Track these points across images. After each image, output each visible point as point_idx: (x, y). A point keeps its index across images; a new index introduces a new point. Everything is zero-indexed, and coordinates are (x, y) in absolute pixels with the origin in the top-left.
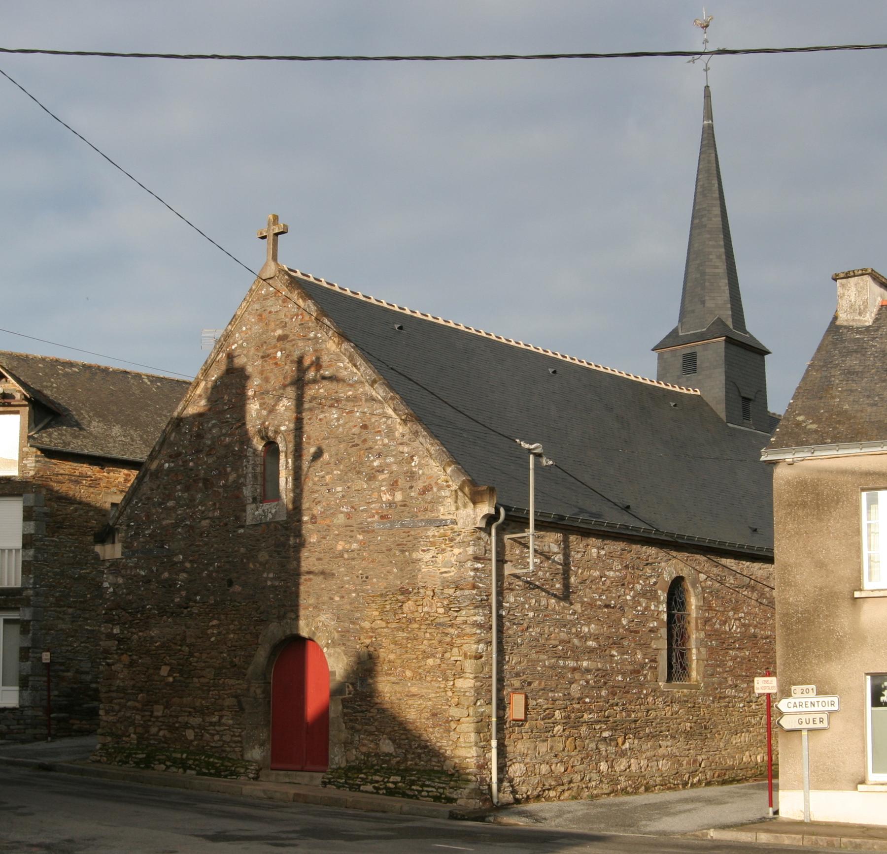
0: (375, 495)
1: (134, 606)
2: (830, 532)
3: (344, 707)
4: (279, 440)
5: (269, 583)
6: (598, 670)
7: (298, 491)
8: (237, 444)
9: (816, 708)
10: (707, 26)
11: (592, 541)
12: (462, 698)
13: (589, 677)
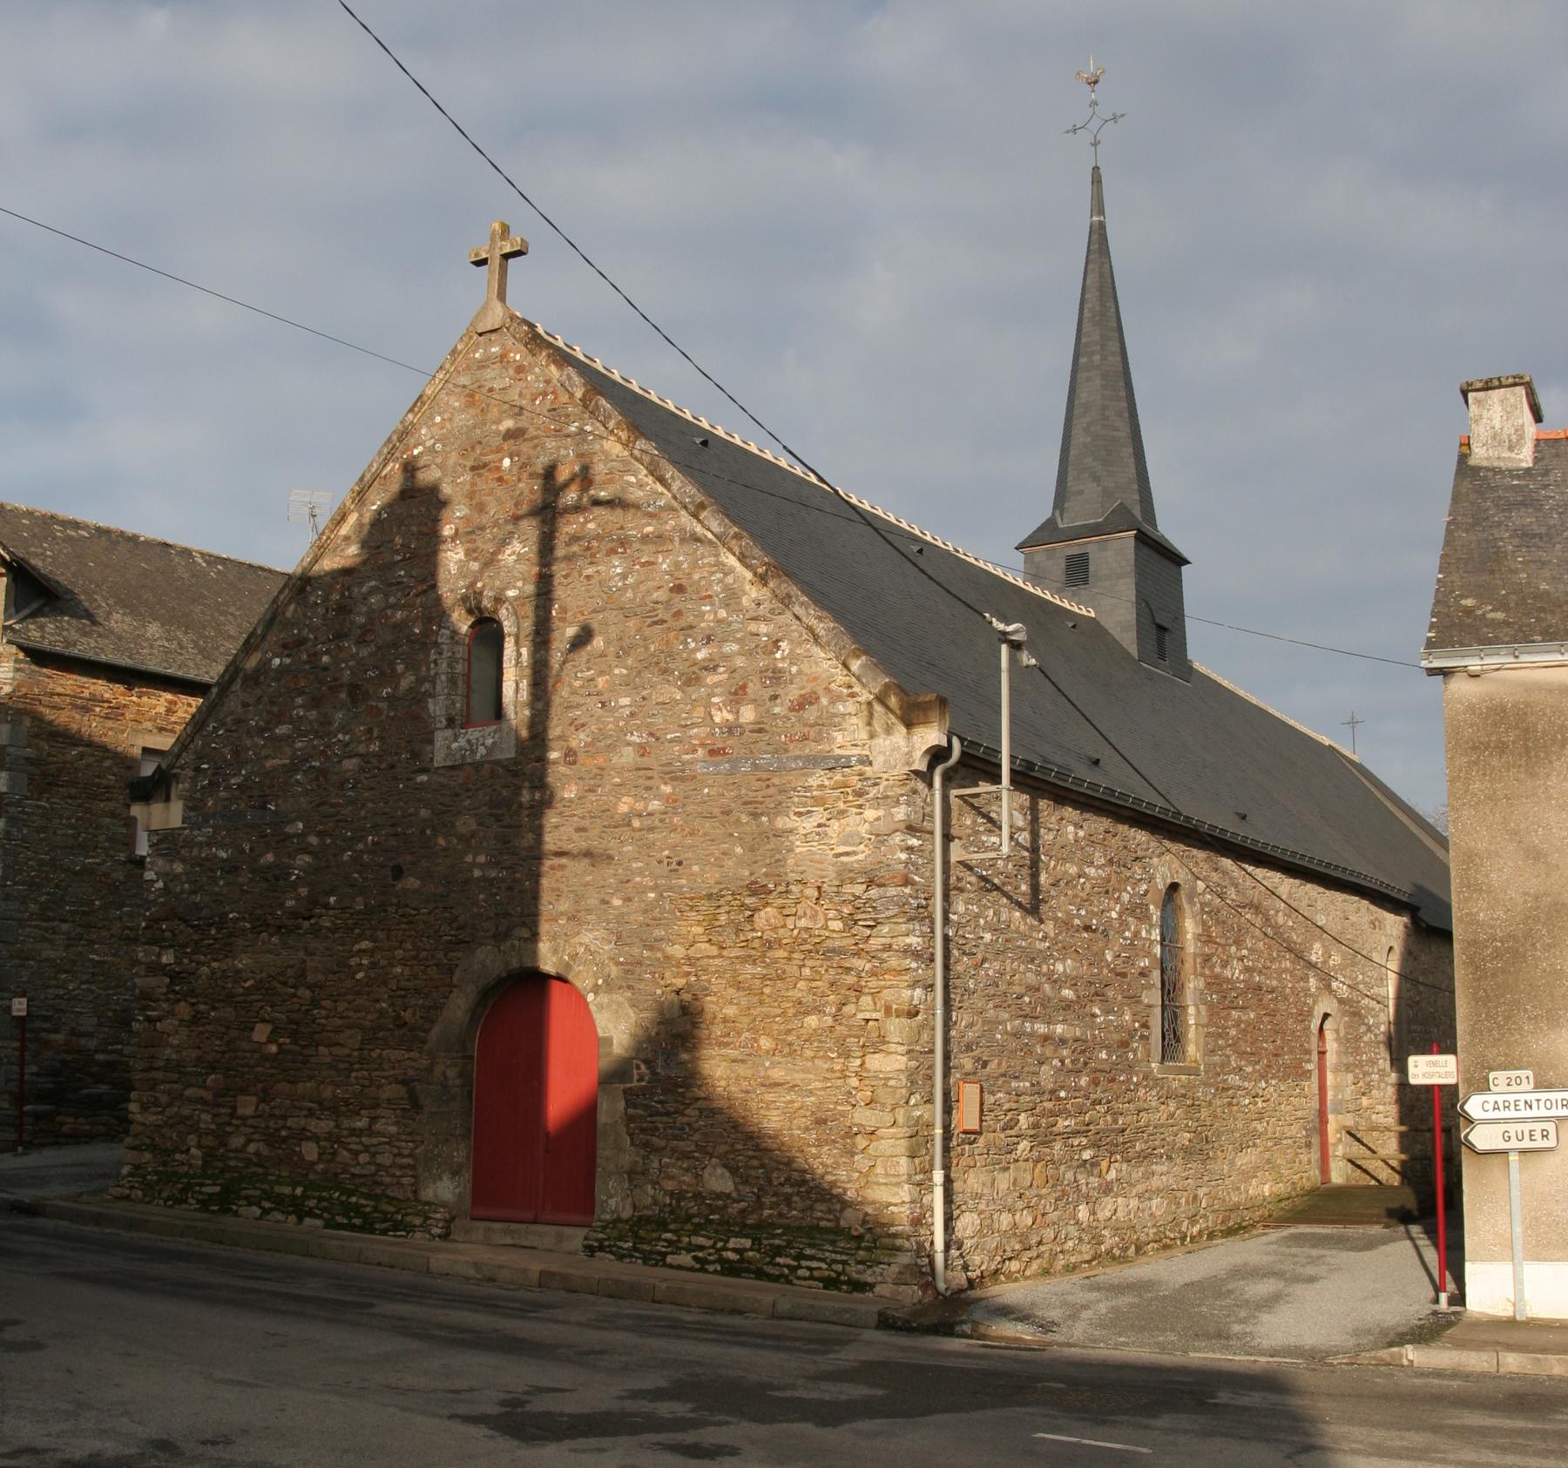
0: (699, 712)
1: (203, 914)
2: (1550, 798)
3: (629, 1104)
4: (503, 613)
5: (477, 873)
6: (1077, 1040)
7: (540, 706)
8: (419, 622)
9: (1535, 1113)
10: (1096, 82)
11: (1069, 812)
12: (880, 1091)
13: (1065, 1053)
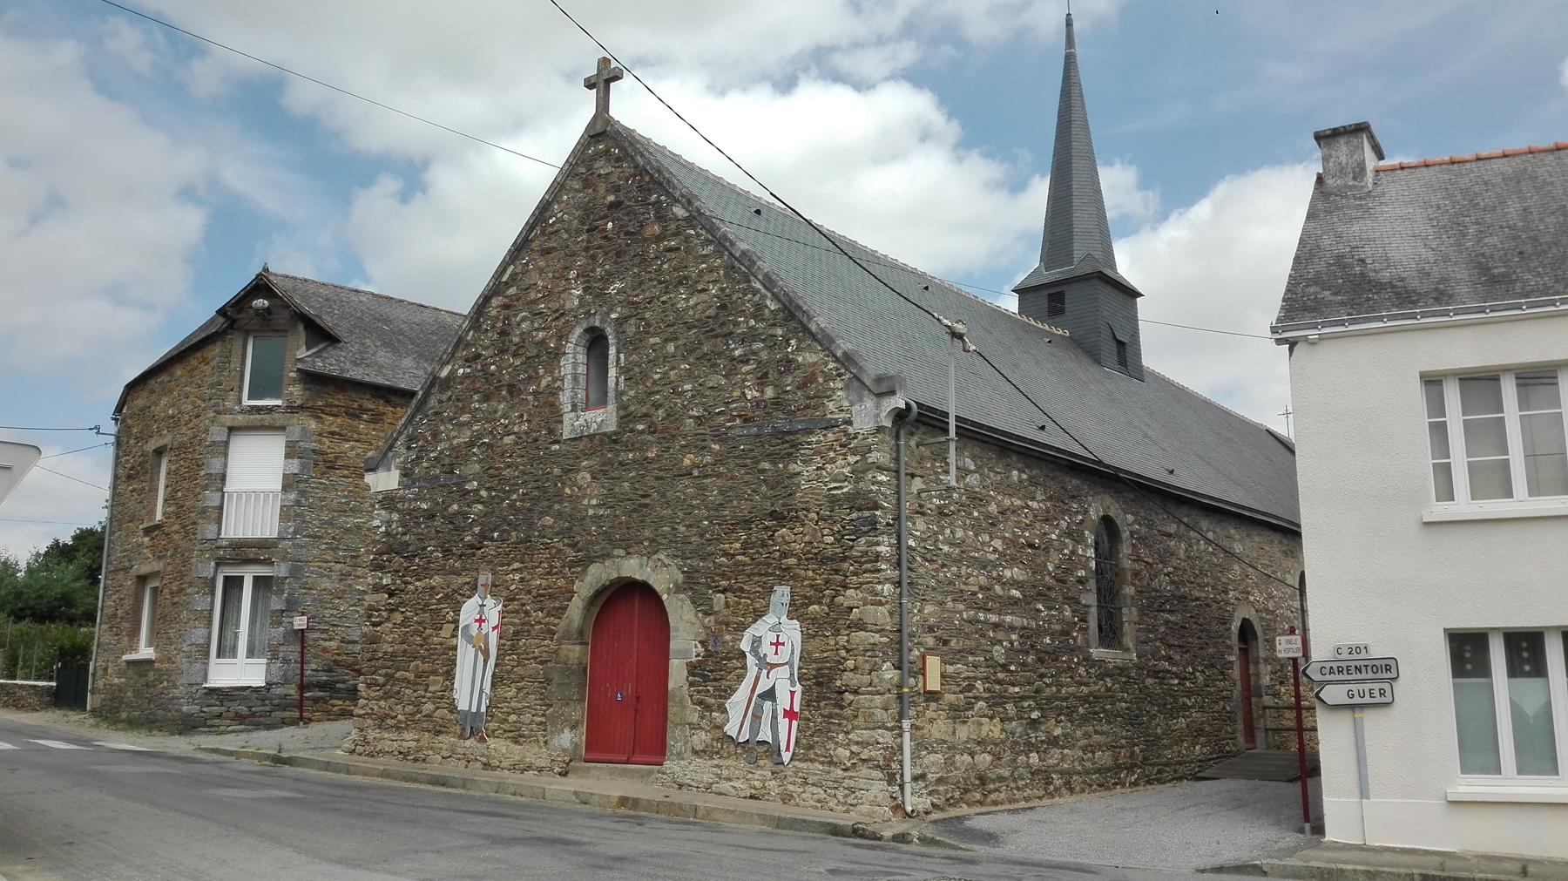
5: (591, 512)
9: (1364, 676)
